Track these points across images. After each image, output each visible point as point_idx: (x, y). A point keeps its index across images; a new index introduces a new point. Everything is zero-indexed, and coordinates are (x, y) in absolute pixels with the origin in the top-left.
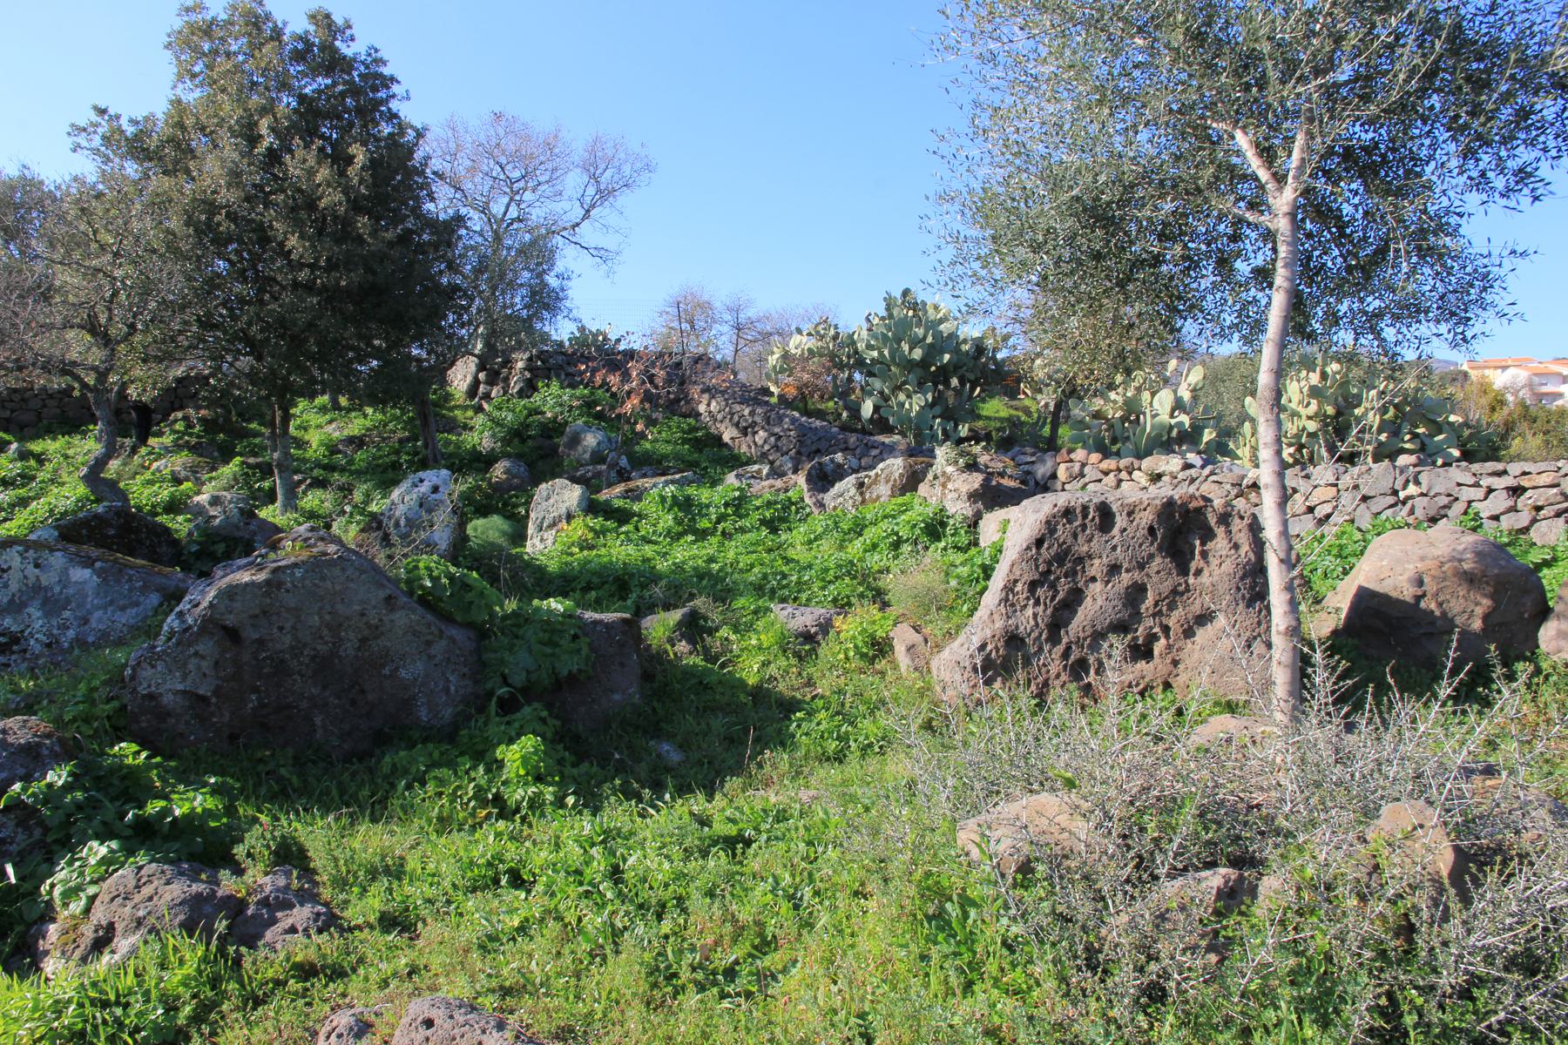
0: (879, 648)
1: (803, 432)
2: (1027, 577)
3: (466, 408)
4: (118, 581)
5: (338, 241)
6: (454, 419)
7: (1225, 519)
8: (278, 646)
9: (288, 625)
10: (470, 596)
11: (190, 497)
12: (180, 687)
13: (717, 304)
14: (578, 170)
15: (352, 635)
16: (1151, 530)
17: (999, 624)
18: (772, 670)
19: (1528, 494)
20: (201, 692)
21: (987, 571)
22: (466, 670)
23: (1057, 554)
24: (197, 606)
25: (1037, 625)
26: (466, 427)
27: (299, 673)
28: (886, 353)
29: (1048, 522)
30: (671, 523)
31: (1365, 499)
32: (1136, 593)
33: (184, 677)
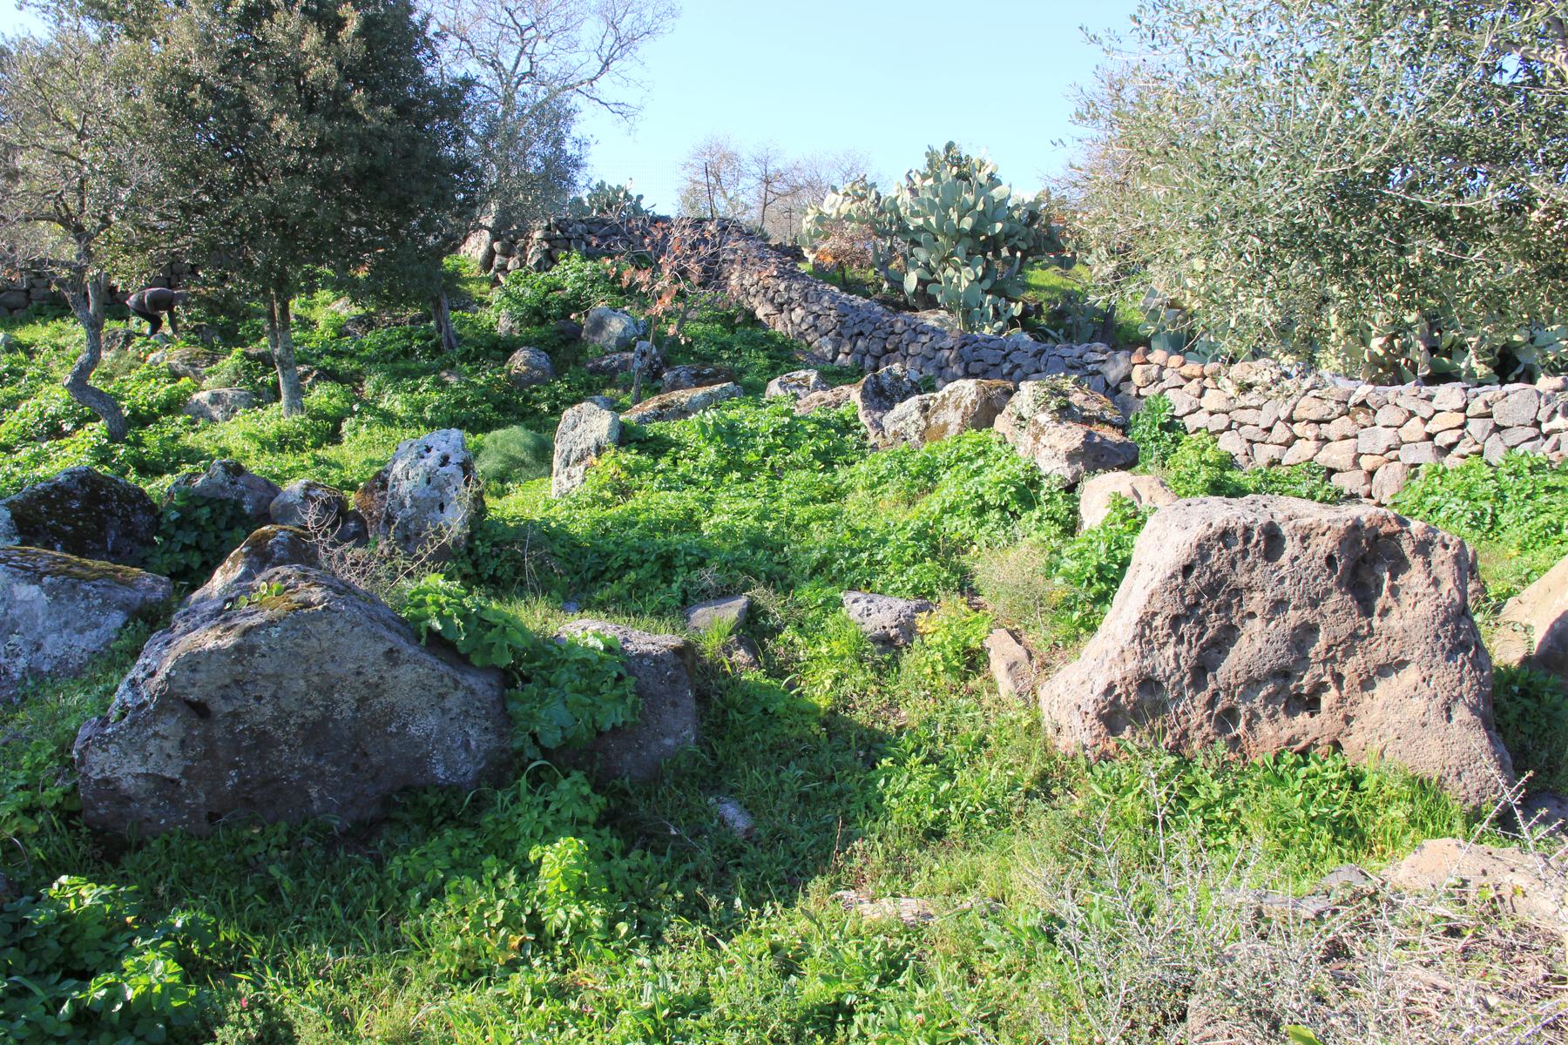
0: (973, 660)
1: (845, 311)
2: (1170, 611)
3: (482, 280)
4: (72, 599)
5: (329, 118)
6: (469, 294)
7: (1424, 548)
8: (257, 718)
9: (267, 695)
10: (490, 636)
11: (189, 394)
12: (142, 770)
13: (744, 156)
14: (595, 18)
15: (347, 697)
16: (1330, 560)
18: (848, 687)
20: (167, 775)
21: (1110, 576)
22: (488, 724)
23: (1209, 584)
24: (152, 674)
25: (1178, 667)
26: (481, 303)
27: (286, 742)
28: (933, 220)
29: (1199, 546)
30: (713, 457)
31: (1498, 429)
32: (1307, 632)
33: (145, 760)
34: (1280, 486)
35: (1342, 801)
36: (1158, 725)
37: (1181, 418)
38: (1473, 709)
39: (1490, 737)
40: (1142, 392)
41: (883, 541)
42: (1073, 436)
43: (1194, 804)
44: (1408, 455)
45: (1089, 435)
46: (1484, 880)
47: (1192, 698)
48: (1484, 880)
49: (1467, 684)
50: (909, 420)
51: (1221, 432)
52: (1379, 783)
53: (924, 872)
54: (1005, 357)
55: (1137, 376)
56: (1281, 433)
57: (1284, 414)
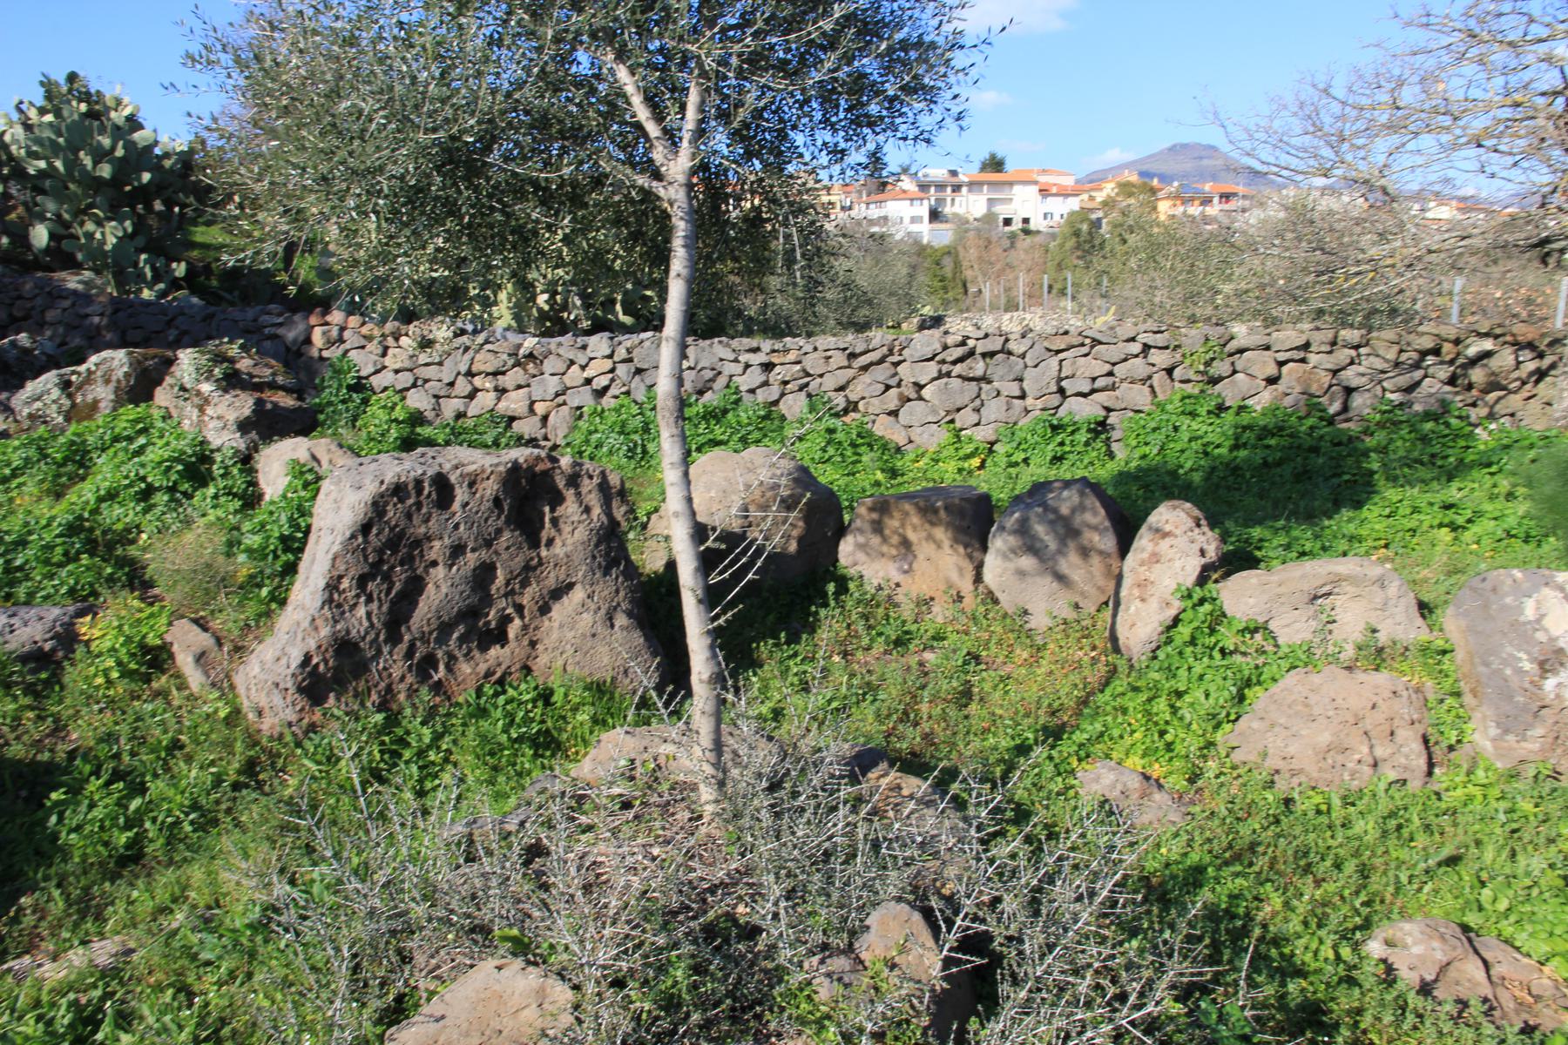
7: (574, 480)
16: (497, 502)
17: (325, 631)
19: (777, 369)
21: (294, 544)
23: (389, 540)
25: (372, 625)
29: (375, 504)
31: (639, 371)
32: (484, 573)
34: (467, 437)
35: (538, 718)
36: (362, 685)
37: (367, 378)
38: (630, 614)
39: (645, 635)
40: (325, 354)
41: (22, 543)
42: (243, 404)
43: (407, 754)
44: (574, 399)
45: (259, 403)
46: (646, 756)
47: (391, 653)
48: (646, 756)
49: (622, 594)
50: (48, 399)
51: (408, 389)
52: (566, 695)
53: (121, 906)
54: (169, 323)
55: (317, 337)
56: (463, 386)
57: (463, 368)
